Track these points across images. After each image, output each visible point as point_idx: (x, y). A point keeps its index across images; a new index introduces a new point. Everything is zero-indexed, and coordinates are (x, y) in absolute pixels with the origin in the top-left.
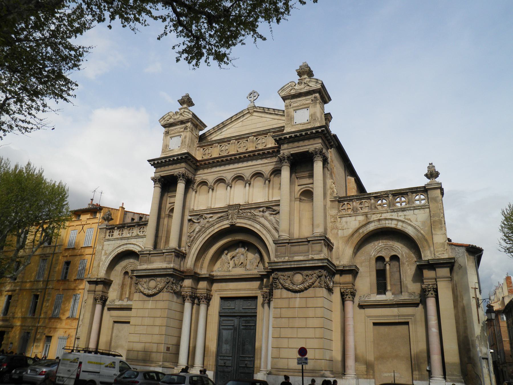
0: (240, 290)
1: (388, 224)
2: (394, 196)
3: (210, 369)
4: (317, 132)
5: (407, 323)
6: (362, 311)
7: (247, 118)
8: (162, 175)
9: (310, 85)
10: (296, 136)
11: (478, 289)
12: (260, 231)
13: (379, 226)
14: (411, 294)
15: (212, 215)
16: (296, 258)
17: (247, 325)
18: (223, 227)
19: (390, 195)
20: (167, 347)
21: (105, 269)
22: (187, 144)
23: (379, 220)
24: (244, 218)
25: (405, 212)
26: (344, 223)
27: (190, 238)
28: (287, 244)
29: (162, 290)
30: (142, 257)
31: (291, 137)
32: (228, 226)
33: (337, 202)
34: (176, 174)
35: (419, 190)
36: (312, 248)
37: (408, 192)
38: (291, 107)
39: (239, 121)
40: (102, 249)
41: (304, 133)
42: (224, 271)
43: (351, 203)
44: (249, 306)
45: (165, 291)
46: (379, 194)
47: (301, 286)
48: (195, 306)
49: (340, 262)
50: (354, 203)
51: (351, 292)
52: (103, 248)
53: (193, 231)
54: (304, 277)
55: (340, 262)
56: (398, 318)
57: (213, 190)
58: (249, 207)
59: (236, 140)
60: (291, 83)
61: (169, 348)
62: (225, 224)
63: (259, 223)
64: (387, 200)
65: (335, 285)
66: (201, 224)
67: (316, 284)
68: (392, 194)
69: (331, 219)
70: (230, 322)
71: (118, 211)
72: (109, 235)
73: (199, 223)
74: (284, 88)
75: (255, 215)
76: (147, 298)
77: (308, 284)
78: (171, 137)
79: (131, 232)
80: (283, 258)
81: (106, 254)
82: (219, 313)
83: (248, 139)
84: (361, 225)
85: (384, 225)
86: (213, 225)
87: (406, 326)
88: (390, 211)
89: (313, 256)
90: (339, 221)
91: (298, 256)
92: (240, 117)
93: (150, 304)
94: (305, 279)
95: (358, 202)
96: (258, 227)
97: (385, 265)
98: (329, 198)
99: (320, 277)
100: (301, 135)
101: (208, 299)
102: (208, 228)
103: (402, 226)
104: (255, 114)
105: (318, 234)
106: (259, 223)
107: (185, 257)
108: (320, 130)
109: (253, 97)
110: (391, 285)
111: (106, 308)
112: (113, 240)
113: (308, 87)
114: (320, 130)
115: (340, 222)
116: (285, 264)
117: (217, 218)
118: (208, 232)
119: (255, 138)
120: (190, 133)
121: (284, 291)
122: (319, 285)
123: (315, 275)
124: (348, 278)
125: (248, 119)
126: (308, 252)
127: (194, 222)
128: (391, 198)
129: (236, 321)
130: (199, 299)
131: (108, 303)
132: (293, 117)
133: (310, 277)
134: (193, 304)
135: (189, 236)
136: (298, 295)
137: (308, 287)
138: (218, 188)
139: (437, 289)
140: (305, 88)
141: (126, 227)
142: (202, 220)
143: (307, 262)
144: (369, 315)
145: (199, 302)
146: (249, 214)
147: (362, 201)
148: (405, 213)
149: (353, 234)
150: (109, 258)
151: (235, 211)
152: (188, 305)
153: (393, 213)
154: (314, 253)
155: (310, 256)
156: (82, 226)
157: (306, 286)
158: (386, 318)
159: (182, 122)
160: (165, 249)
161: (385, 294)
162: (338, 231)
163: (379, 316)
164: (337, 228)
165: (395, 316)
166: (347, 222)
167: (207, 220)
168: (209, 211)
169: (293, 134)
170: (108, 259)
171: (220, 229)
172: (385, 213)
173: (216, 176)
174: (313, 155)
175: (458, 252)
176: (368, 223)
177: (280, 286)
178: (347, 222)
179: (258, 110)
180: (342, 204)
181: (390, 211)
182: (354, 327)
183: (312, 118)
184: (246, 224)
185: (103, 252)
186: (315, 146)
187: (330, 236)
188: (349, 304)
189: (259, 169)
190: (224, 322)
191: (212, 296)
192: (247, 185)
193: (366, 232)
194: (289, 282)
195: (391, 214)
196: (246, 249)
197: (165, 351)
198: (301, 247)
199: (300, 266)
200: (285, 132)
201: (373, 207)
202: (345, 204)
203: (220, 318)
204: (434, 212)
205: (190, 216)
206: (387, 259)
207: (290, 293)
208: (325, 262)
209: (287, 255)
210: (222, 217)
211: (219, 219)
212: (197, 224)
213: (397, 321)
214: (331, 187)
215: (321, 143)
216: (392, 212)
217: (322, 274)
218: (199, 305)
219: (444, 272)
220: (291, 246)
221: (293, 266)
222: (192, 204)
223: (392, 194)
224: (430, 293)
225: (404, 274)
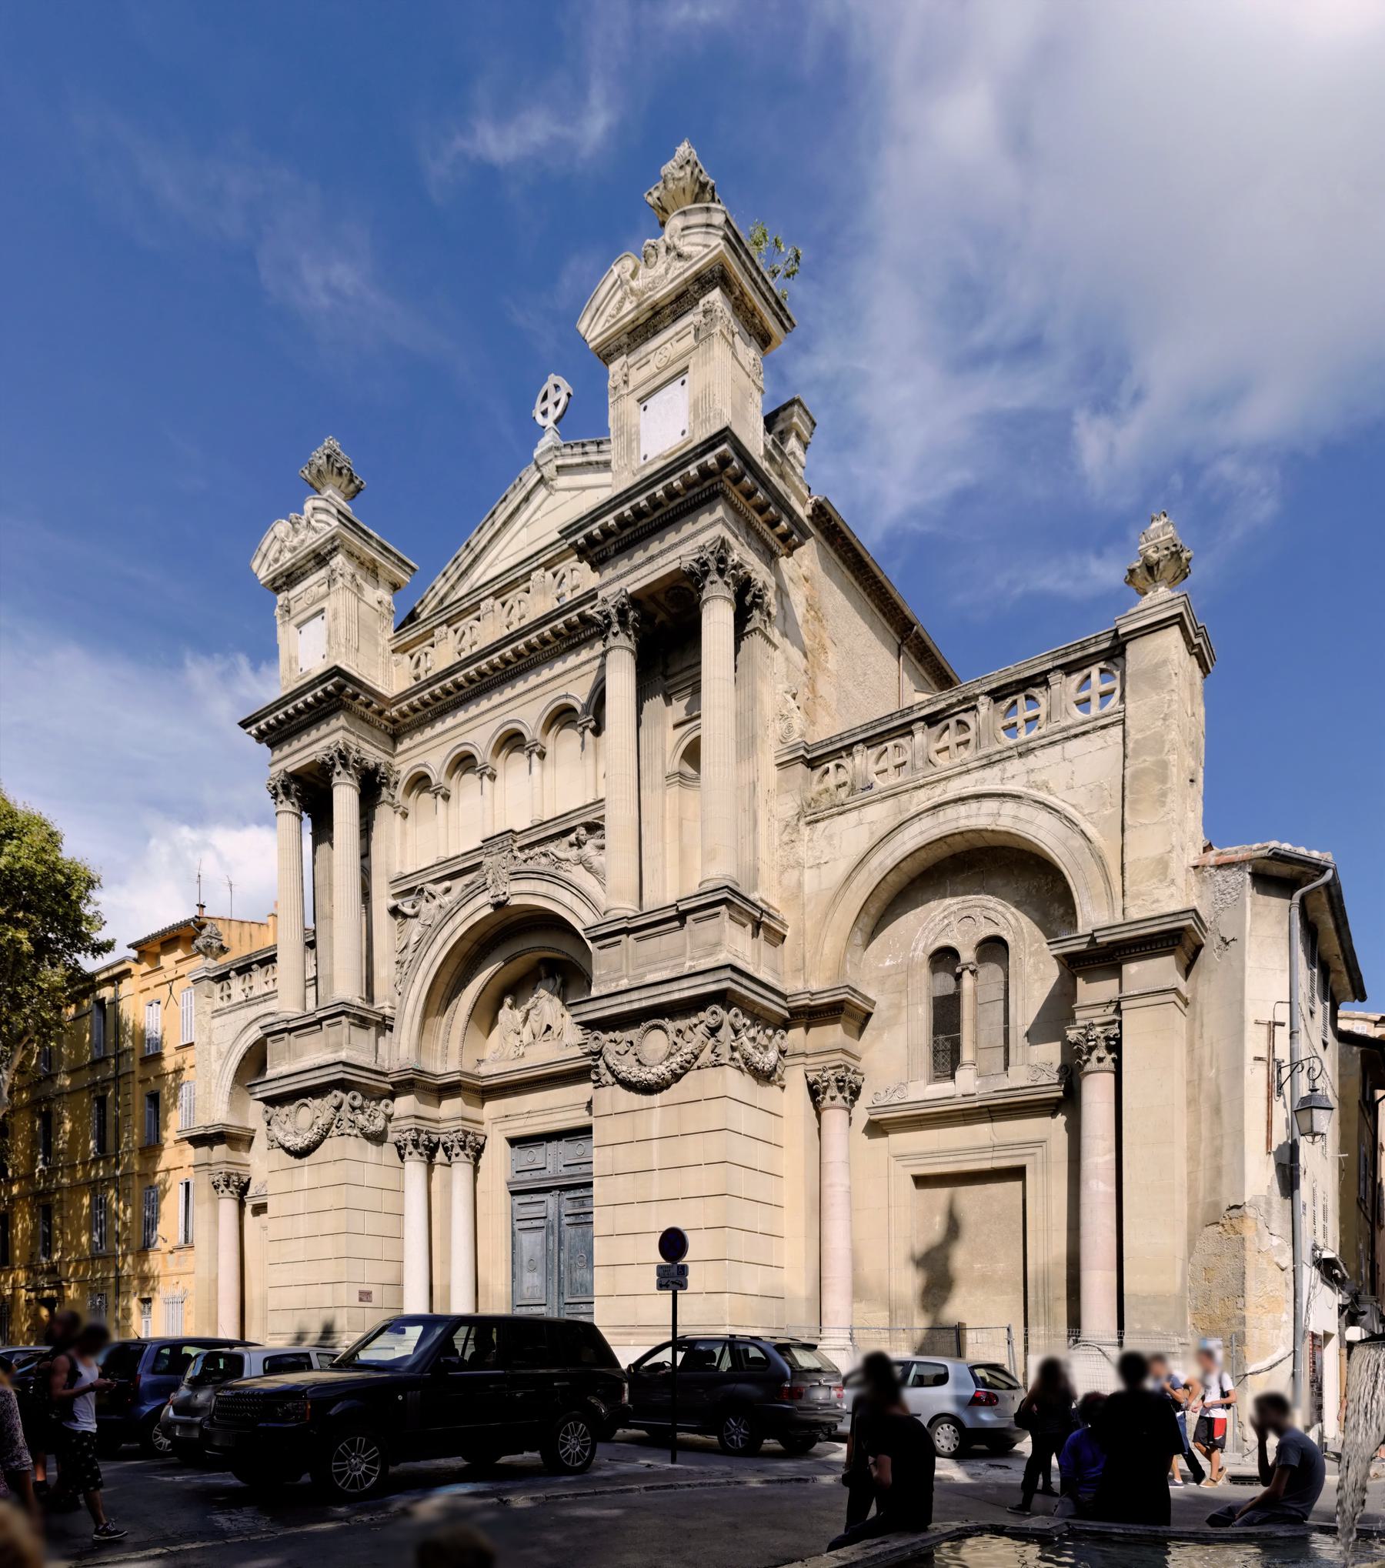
0: (551, 1110)
1: (968, 817)
2: (996, 700)
5: (1017, 1173)
6: (880, 1142)
7: (539, 508)
8: (289, 770)
9: (686, 250)
10: (638, 513)
11: (1286, 1029)
14: (1035, 1068)
15: (447, 884)
19: (982, 698)
20: (361, 1293)
21: (226, 1099)
22: (343, 641)
25: (1031, 757)
27: (402, 967)
28: (623, 937)
29: (328, 1130)
30: (273, 1042)
31: (622, 522)
32: (489, 910)
33: (800, 768)
34: (320, 756)
35: (1092, 650)
37: (1048, 671)
38: (631, 388)
40: (210, 1043)
43: (846, 762)
45: (334, 1134)
49: (806, 981)
50: (858, 759)
51: (838, 1080)
52: (210, 1038)
53: (405, 947)
54: (673, 1037)
55: (806, 981)
56: (989, 1155)
59: (497, 595)
61: (369, 1294)
62: (480, 908)
63: (569, 885)
65: (787, 1062)
66: (422, 917)
67: (706, 1056)
68: (988, 693)
70: (535, 1208)
71: (264, 928)
72: (222, 998)
76: (298, 1162)
77: (679, 1059)
78: (299, 626)
79: (270, 978)
80: (613, 985)
81: (220, 1053)
83: (530, 583)
86: (450, 915)
87: (1017, 1185)
90: (806, 839)
93: (306, 1172)
94: (675, 1044)
95: (872, 754)
97: (958, 977)
99: (713, 1031)
102: (441, 926)
103: (1015, 817)
104: (563, 481)
106: (569, 885)
107: (391, 1029)
110: (977, 1048)
111: (248, 1209)
112: (230, 1012)
118: (440, 940)
119: (549, 574)
120: (349, 594)
122: (713, 1057)
123: (702, 1027)
124: (833, 1034)
127: (405, 916)
131: (251, 1192)
132: (638, 433)
133: (688, 1034)
135: (397, 962)
136: (657, 1099)
139: (1119, 1041)
141: (254, 966)
142: (422, 905)
144: (898, 1152)
146: (543, 860)
147: (887, 744)
148: (1031, 761)
150: (230, 1063)
156: (167, 986)
157: (674, 1066)
158: (951, 1159)
159: (320, 559)
160: (320, 1007)
161: (953, 1077)
162: (801, 874)
163: (932, 1154)
164: (799, 865)
165: (981, 1149)
167: (437, 902)
170: (228, 1068)
175: (1223, 887)
177: (610, 1078)
182: (849, 1192)
183: (696, 416)
185: (214, 1049)
188: (834, 1118)
192: (535, 757)
193: (890, 863)
194: (630, 1059)
196: (559, 981)
197: (355, 1301)
201: (920, 764)
202: (827, 771)
204: (1139, 736)
205: (395, 896)
206: (967, 955)
213: (986, 1165)
214: (785, 712)
215: (721, 520)
217: (719, 1019)
219: (1159, 970)
220: (638, 939)
222: (398, 859)
223: (988, 693)
224: (1095, 1054)
225: (1020, 1003)
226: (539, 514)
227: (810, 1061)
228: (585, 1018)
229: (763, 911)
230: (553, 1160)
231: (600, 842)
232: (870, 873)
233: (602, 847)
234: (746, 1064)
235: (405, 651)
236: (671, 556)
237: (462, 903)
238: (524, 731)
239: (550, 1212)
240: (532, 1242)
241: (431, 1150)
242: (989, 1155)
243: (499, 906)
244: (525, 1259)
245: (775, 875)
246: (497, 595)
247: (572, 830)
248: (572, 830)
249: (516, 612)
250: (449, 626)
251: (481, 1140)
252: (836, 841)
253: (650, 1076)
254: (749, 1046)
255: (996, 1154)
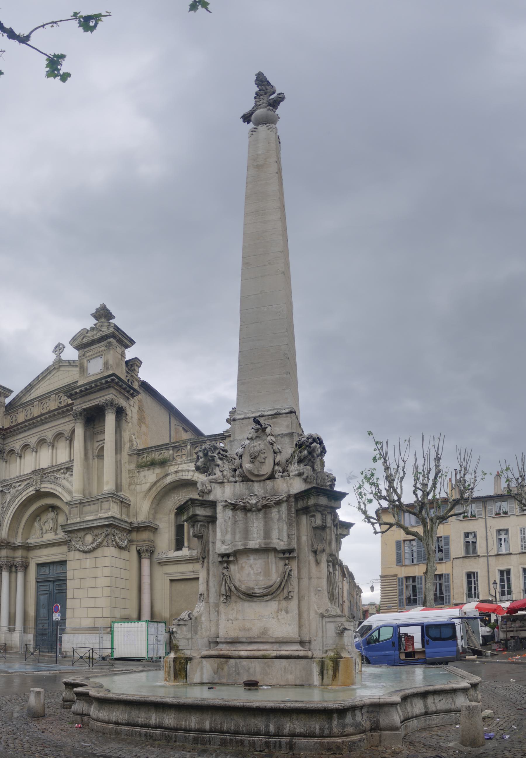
0: (52, 555)
1: (185, 475)
3: (31, 632)
4: (107, 382)
9: (103, 330)
12: (61, 493)
13: (176, 479)
15: (20, 483)
16: (87, 518)
17: (59, 588)
18: (30, 494)
19: (189, 444)
23: (176, 472)
24: (48, 482)
26: (142, 478)
27: (4, 509)
31: (81, 391)
32: (34, 492)
33: (136, 456)
35: (218, 437)
36: (101, 506)
37: (206, 440)
39: (47, 379)
41: (93, 385)
42: (38, 538)
44: (61, 570)
46: (177, 444)
47: (90, 547)
48: (13, 575)
53: (5, 502)
56: (192, 574)
57: (20, 457)
58: (52, 470)
60: (83, 331)
62: (31, 491)
63: (61, 486)
64: (186, 450)
66: (11, 493)
67: (105, 543)
68: (191, 443)
69: (129, 474)
70: (45, 587)
73: (9, 493)
74: (76, 338)
75: (58, 478)
77: (96, 544)
80: (75, 520)
82: (36, 579)
84: (158, 478)
85: (181, 477)
86: (21, 493)
88: (187, 461)
89: (101, 515)
91: (89, 516)
92: (47, 374)
96: (60, 489)
98: (125, 454)
100: (91, 387)
101: (25, 567)
103: (198, 477)
105: (107, 492)
106: (61, 486)
108: (109, 379)
109: (58, 350)
113: (101, 332)
114: (109, 379)
115: (139, 477)
116: (75, 526)
117: (25, 486)
121: (77, 553)
124: (145, 535)
125: (55, 375)
126: (98, 511)
127: (6, 493)
128: (189, 447)
129: (51, 585)
130: (16, 567)
134: (11, 572)
135: (2, 507)
136: (89, 555)
137: (96, 546)
138: (25, 455)
140: (98, 334)
143: (95, 522)
145: (17, 570)
146: (52, 478)
147: (162, 452)
149: (150, 489)
151: (38, 476)
152: (5, 574)
153: (190, 464)
154: (102, 511)
155: (99, 515)
157: (94, 546)
162: (136, 487)
165: (190, 572)
166: (145, 476)
167: (16, 489)
168: (17, 479)
169: (83, 388)
171: (27, 496)
172: (183, 464)
173: (22, 442)
174: (105, 408)
176: (167, 475)
178: (145, 476)
179: (64, 364)
180: (141, 457)
181: (187, 461)
184: (49, 488)
186: (106, 397)
187: (125, 493)
189: (60, 429)
190: (41, 587)
191: (29, 563)
193: (163, 486)
195: (188, 464)
196: (56, 513)
198: (92, 506)
199: (89, 526)
200: (78, 384)
203: (37, 584)
205: (2, 487)
207: (82, 554)
208: (110, 520)
209: (79, 516)
210: (28, 484)
211: (27, 486)
212: (8, 494)
216: (189, 463)
218: (16, 572)
221: (82, 527)
223: (191, 443)
226: (53, 377)
227: (138, 543)
228: (66, 530)
229: (123, 498)
230: (52, 572)
231: (71, 473)
232: (157, 488)
233: (72, 475)
234: (117, 545)
235: (8, 415)
236: (97, 400)
237: (25, 489)
238: (47, 439)
239: (51, 588)
240: (43, 598)
241: (11, 567)
242: (192, 574)
243: (37, 491)
244: (41, 604)
245: (127, 486)
246: (39, 401)
247: (62, 469)
248: (62, 469)
249: (45, 406)
250: (23, 408)
251: (27, 564)
252: (147, 477)
253: (86, 549)
254: (118, 541)
255: (194, 574)
